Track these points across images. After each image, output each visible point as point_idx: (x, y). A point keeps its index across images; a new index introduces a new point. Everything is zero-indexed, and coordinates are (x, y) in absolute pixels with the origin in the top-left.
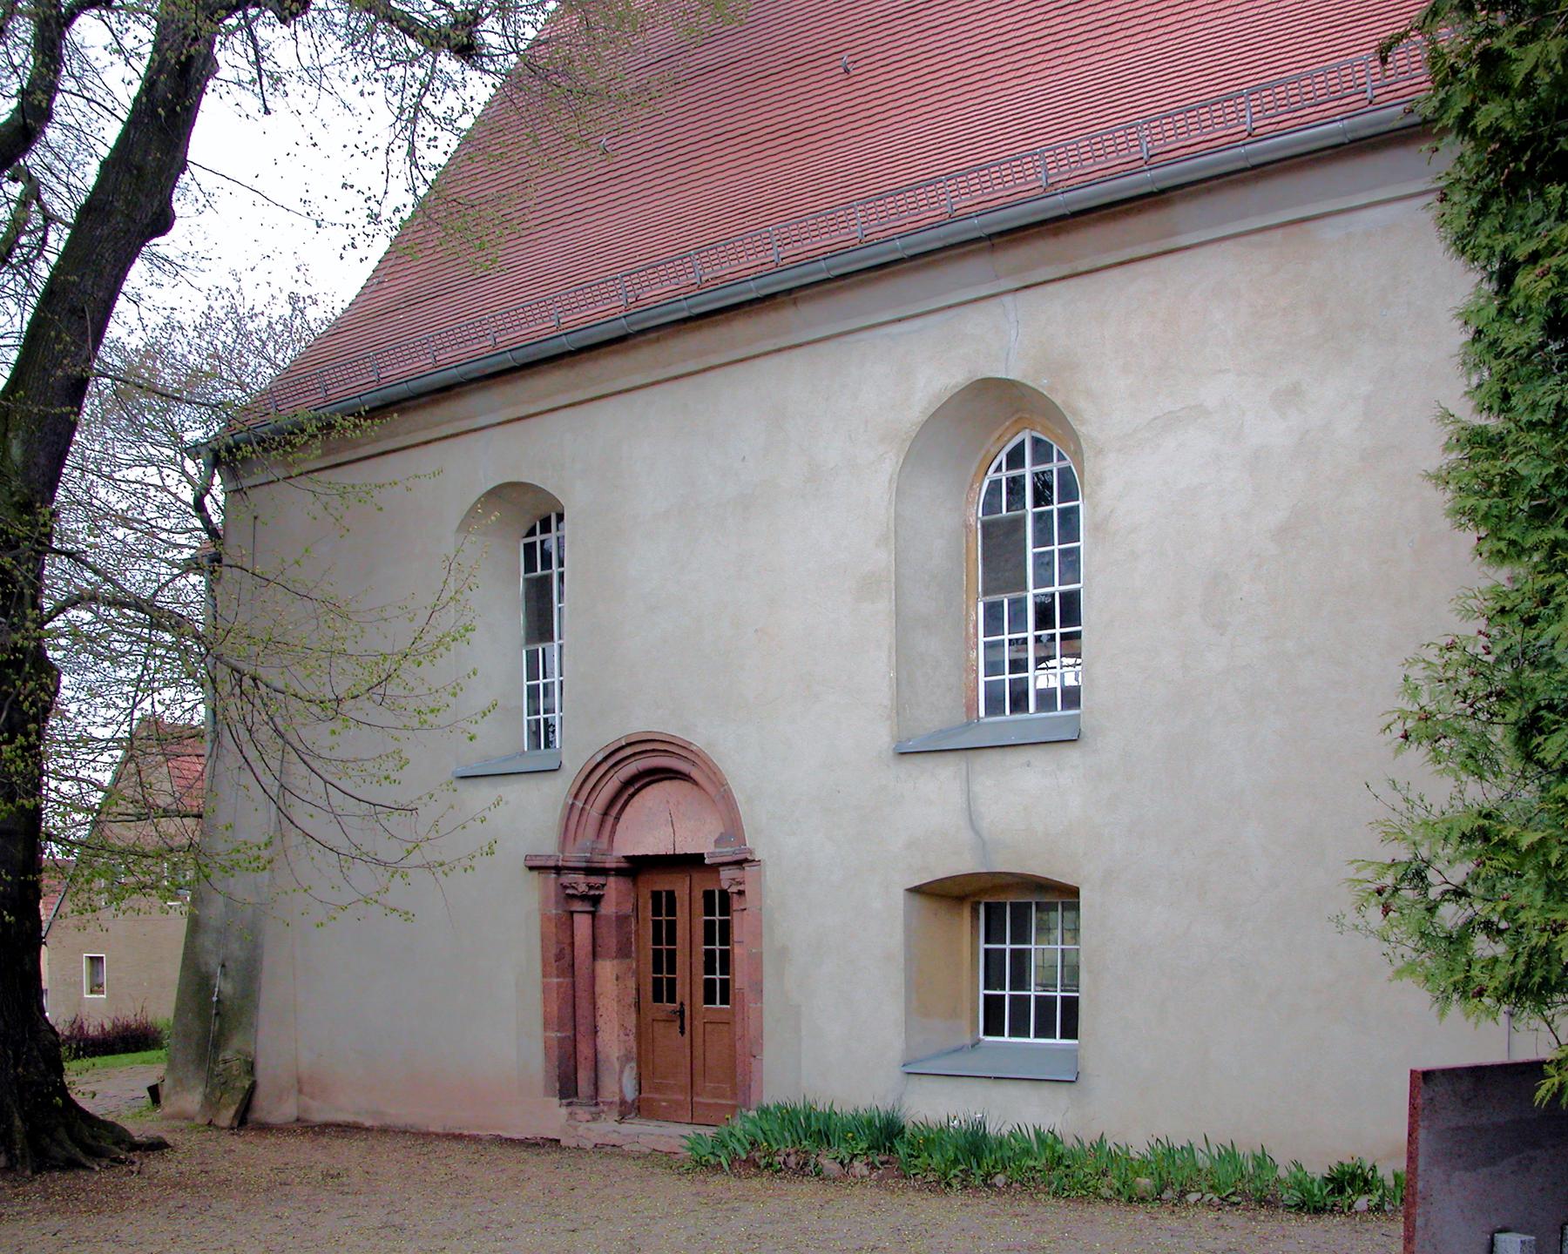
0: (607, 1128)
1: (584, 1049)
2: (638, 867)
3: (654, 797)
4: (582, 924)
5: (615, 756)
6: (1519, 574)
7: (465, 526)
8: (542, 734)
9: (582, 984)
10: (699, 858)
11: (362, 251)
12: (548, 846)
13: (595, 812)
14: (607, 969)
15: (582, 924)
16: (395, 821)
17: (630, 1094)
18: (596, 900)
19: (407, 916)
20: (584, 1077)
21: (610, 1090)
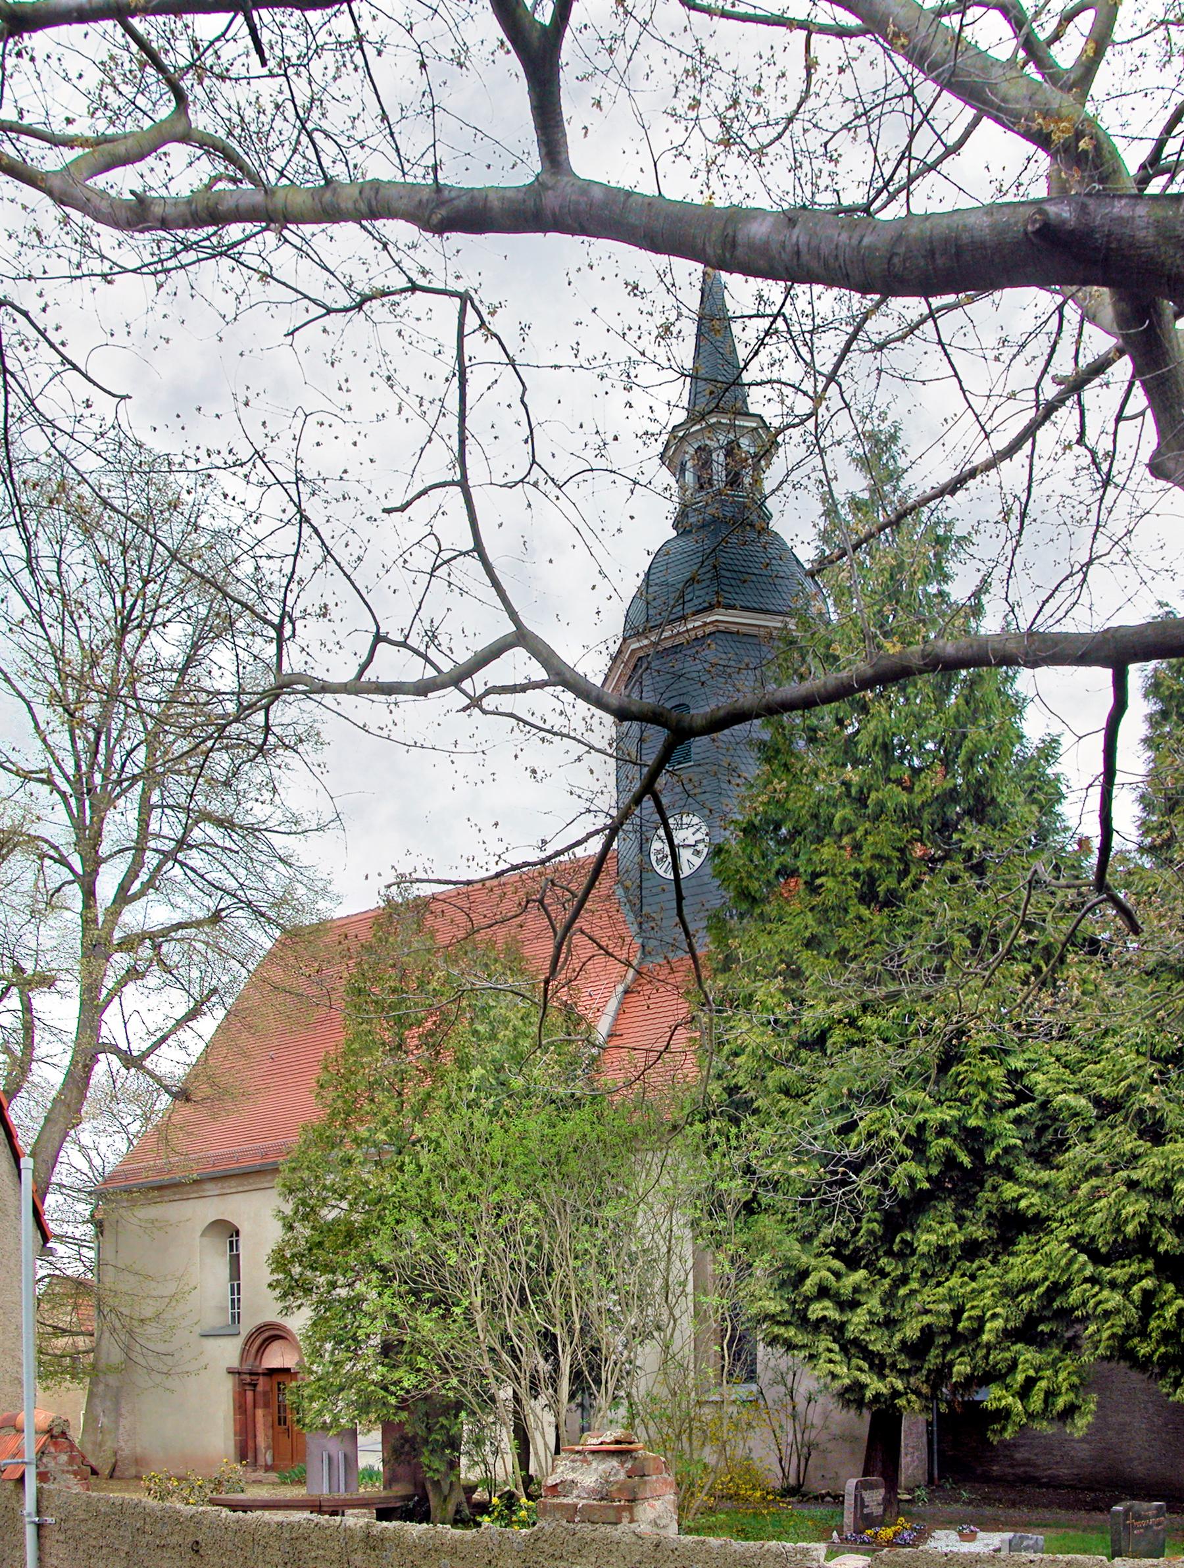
0: (260, 1474)
1: (251, 1443)
2: (272, 1372)
3: (276, 1346)
4: (250, 1394)
5: (260, 1329)
6: (912, 1180)
7: (203, 1235)
8: (236, 1318)
9: (250, 1420)
10: (288, 1370)
11: (592, 46)
12: (235, 1363)
13: (253, 1351)
14: (260, 1412)
15: (250, 1394)
16: (168, 1359)
17: (270, 1462)
18: (255, 1385)
19: (172, 1391)
20: (250, 1454)
21: (261, 1461)
